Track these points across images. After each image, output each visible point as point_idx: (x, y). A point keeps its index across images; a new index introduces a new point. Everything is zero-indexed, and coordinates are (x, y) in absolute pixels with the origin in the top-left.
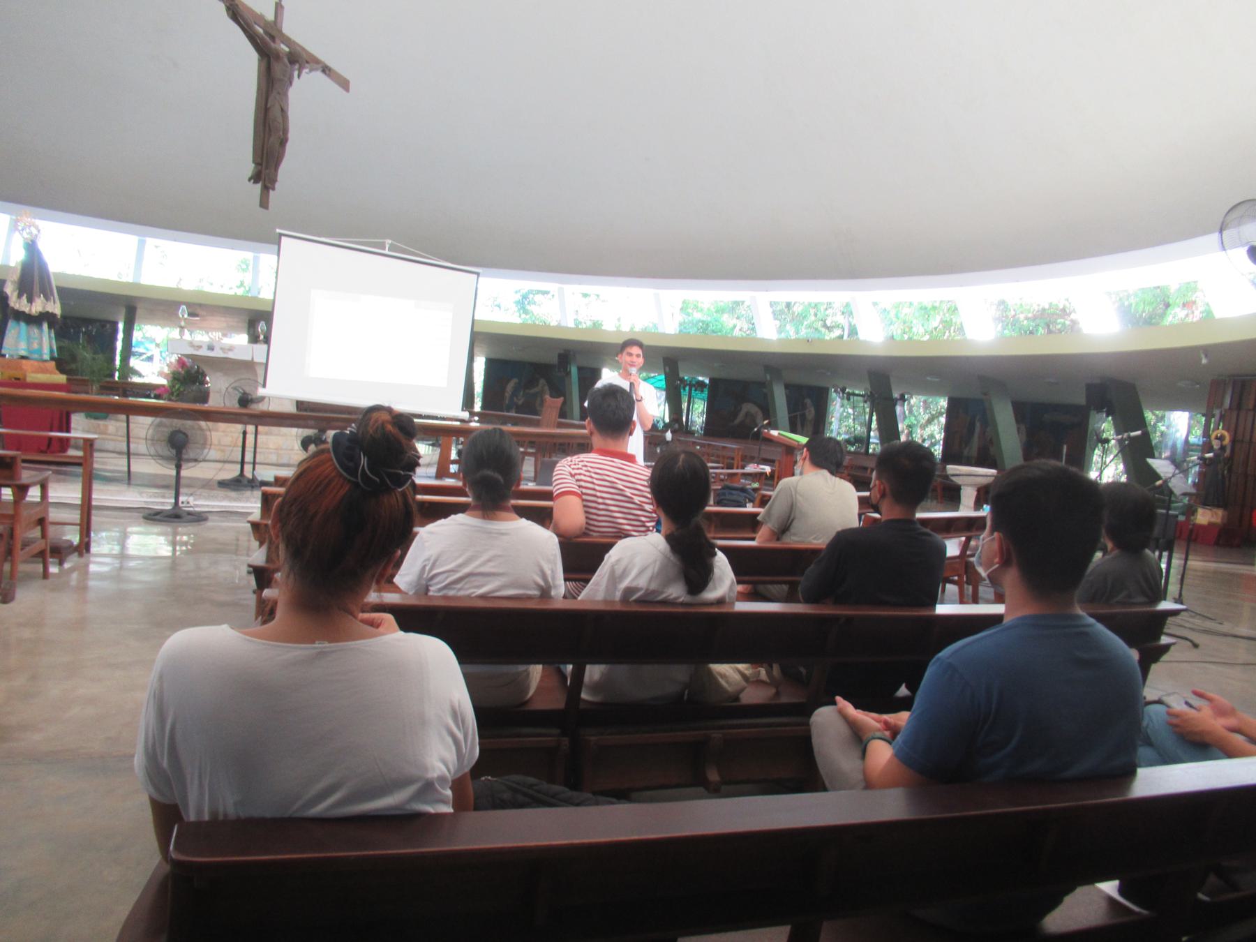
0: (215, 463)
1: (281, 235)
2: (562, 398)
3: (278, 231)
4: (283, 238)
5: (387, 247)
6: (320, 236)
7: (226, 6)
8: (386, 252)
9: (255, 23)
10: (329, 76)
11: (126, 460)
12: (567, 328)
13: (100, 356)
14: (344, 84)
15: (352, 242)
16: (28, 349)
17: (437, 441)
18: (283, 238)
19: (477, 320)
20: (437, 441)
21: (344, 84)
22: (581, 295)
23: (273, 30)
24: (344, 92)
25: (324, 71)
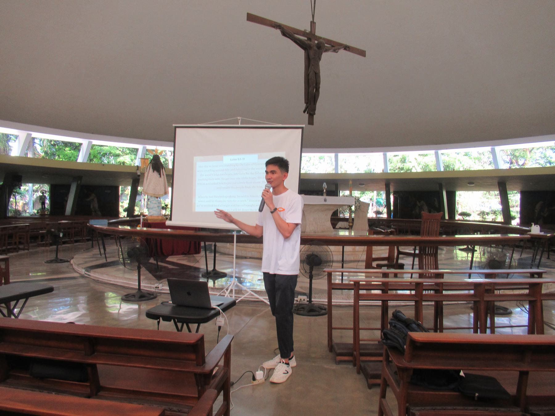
0: (374, 274)
1: (176, 127)
2: (376, 266)
3: (174, 125)
4: (177, 129)
5: (240, 121)
6: (197, 124)
7: (281, 31)
8: (240, 125)
9: (294, 34)
10: (349, 51)
11: (105, 259)
12: (430, 172)
13: (141, 212)
14: (362, 53)
15: (218, 123)
16: (348, 229)
17: (245, 283)
18: (177, 129)
19: (172, 147)
20: (245, 283)
21: (362, 53)
22: (534, 147)
23: (311, 35)
24: (250, 12)
25: (345, 49)
